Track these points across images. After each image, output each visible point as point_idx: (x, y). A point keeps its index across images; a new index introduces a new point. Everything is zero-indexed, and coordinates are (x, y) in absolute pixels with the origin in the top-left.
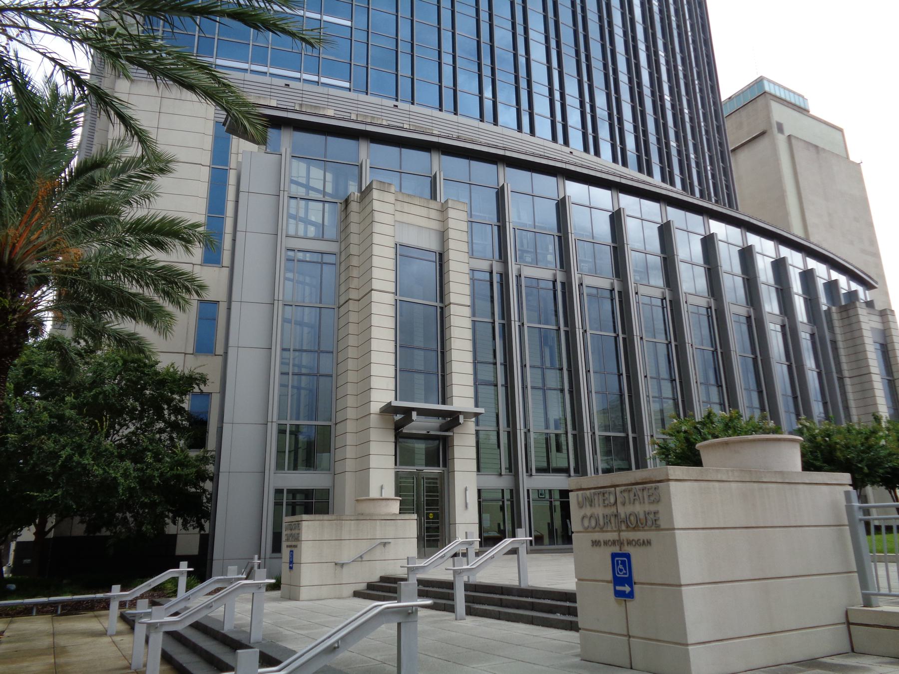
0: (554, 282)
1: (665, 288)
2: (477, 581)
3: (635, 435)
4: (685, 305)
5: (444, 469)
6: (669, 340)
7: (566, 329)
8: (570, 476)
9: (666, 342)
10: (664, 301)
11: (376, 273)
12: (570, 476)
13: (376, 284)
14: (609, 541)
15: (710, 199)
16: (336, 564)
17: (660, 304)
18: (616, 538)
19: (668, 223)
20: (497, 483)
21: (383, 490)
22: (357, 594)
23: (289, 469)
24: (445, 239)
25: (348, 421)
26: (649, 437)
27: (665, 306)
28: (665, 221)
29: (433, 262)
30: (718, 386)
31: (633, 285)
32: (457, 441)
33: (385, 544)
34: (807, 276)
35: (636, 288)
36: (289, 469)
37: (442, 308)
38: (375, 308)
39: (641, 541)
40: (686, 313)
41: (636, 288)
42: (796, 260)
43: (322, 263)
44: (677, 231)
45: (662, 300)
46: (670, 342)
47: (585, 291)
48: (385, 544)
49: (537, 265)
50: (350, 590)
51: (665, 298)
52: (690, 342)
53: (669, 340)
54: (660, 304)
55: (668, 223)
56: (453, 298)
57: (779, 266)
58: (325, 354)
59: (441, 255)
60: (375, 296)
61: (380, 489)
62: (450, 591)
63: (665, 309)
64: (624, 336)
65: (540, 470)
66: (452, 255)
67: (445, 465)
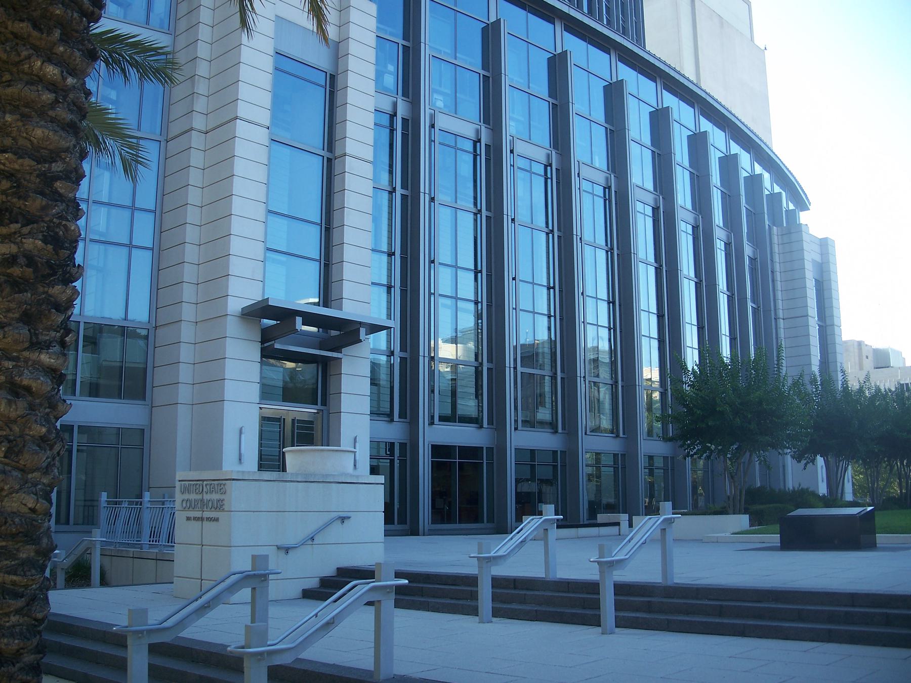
0: (393, 116)
1: (482, 124)
2: (558, 576)
3: (491, 366)
4: (577, 179)
5: (323, 408)
6: (550, 228)
7: (404, 192)
8: (392, 420)
9: (546, 230)
10: (549, 168)
11: (244, 91)
12: (481, 427)
13: (243, 110)
14: (196, 517)
15: (601, 19)
16: (278, 548)
17: (471, 149)
18: (200, 516)
19: (564, 54)
20: (393, 432)
21: (243, 436)
22: (308, 594)
23: (81, 395)
24: (341, 54)
25: (183, 322)
26: (427, 360)
27: (549, 176)
28: (559, 51)
29: (322, 86)
30: (609, 303)
31: (508, 138)
32: (347, 367)
33: (343, 519)
34: (729, 163)
35: (432, 117)
36: (81, 395)
37: (329, 160)
38: (240, 148)
39: (213, 519)
40: (578, 191)
41: (432, 117)
42: (717, 138)
43: (456, 148)
44: (574, 68)
45: (546, 166)
46: (480, 211)
47: (438, 137)
48: (343, 519)
49: (456, 114)
50: (295, 589)
51: (550, 165)
52: (579, 234)
53: (550, 228)
54: (542, 173)
55: (564, 54)
56: (351, 147)
57: (698, 143)
58: (137, 211)
59: (333, 78)
60: (241, 128)
61: (238, 432)
62: (398, 597)
63: (549, 181)
64: (489, 214)
65: (443, 419)
66: (353, 80)
67: (324, 403)
